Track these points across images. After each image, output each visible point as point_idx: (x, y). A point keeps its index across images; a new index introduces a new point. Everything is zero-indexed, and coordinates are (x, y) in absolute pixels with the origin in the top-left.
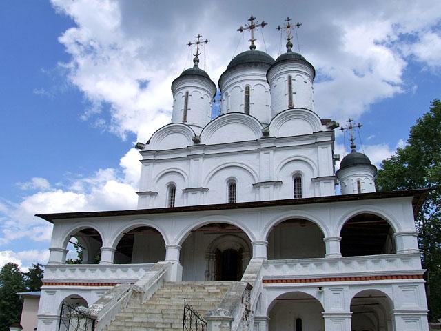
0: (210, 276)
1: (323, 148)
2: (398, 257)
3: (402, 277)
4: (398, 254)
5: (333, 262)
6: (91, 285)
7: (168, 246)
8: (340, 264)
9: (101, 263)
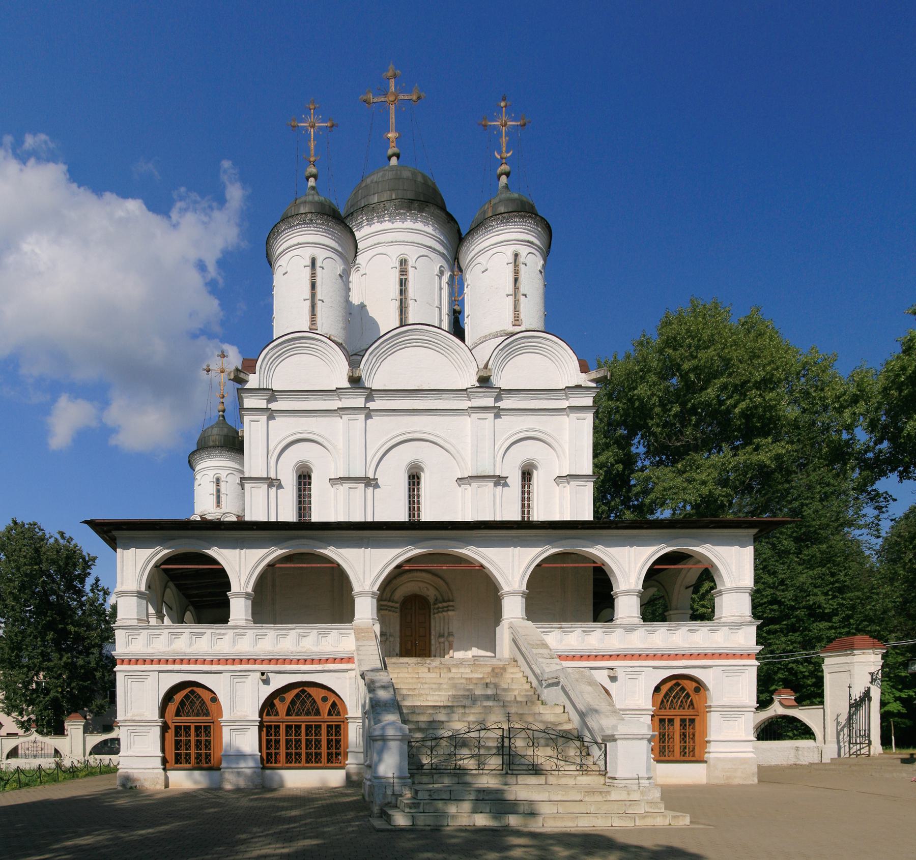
1: (578, 419)
2: (620, 626)
4: (229, 624)
5: (630, 628)
6: (219, 662)
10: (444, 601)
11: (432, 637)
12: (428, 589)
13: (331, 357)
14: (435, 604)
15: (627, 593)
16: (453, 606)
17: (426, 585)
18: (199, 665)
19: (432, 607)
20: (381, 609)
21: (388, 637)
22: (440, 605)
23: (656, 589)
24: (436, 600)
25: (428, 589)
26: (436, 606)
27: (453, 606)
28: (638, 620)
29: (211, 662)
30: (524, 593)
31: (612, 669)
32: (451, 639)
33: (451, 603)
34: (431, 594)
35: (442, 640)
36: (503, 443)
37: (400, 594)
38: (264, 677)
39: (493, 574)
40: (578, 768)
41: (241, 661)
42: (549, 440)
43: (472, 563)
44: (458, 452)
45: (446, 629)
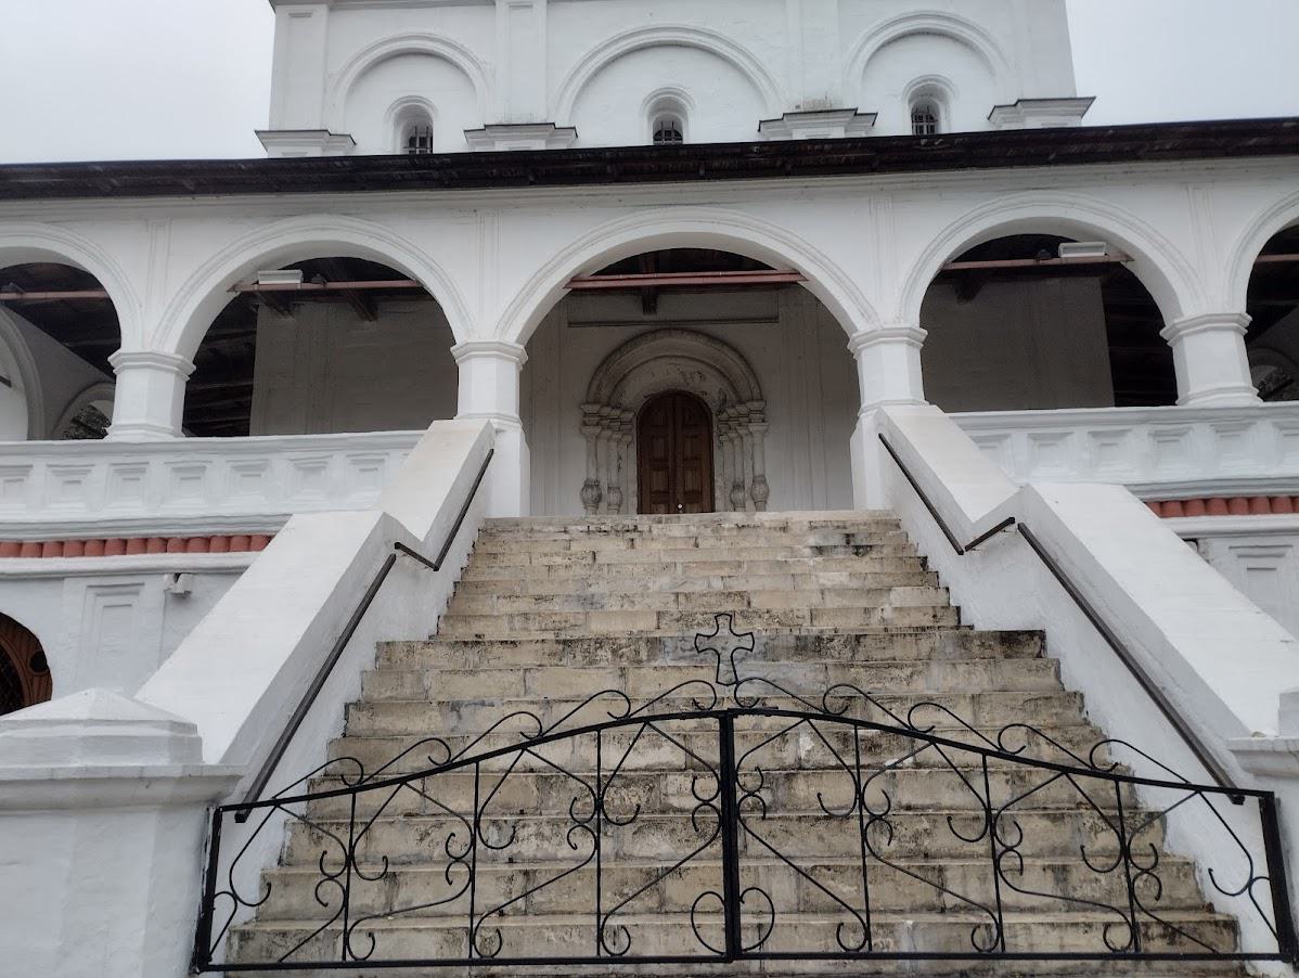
0: (603, 505)
3: (102, 546)
5: (1228, 423)
6: (61, 548)
7: (470, 348)
8: (1264, 434)
9: (114, 435)
10: (741, 402)
11: (718, 494)
12: (702, 377)
13: (788, 235)
14: (721, 412)
15: (1210, 323)
16: (761, 412)
17: (701, 367)
18: (29, 560)
19: (714, 418)
20: (585, 424)
21: (605, 492)
22: (731, 411)
23: (1274, 368)
24: (725, 400)
25: (702, 377)
26: (725, 416)
27: (761, 412)
28: (1249, 398)
29: (40, 549)
30: (910, 334)
31: (1195, 540)
32: (759, 489)
33: (756, 405)
34: (711, 388)
35: (740, 495)
36: (862, 47)
37: (637, 389)
38: (179, 588)
39: (831, 297)
40: (1120, 937)
41: (124, 546)
42: (967, 34)
43: (759, 266)
44: (759, 69)
45: (748, 471)
